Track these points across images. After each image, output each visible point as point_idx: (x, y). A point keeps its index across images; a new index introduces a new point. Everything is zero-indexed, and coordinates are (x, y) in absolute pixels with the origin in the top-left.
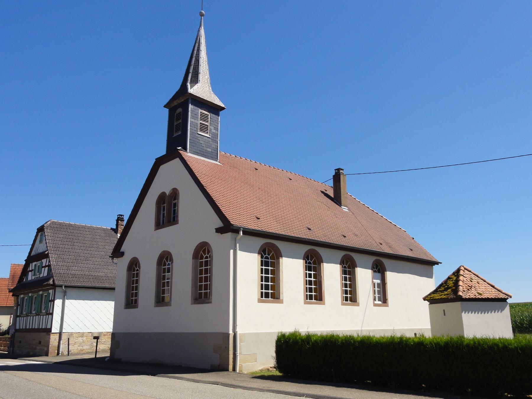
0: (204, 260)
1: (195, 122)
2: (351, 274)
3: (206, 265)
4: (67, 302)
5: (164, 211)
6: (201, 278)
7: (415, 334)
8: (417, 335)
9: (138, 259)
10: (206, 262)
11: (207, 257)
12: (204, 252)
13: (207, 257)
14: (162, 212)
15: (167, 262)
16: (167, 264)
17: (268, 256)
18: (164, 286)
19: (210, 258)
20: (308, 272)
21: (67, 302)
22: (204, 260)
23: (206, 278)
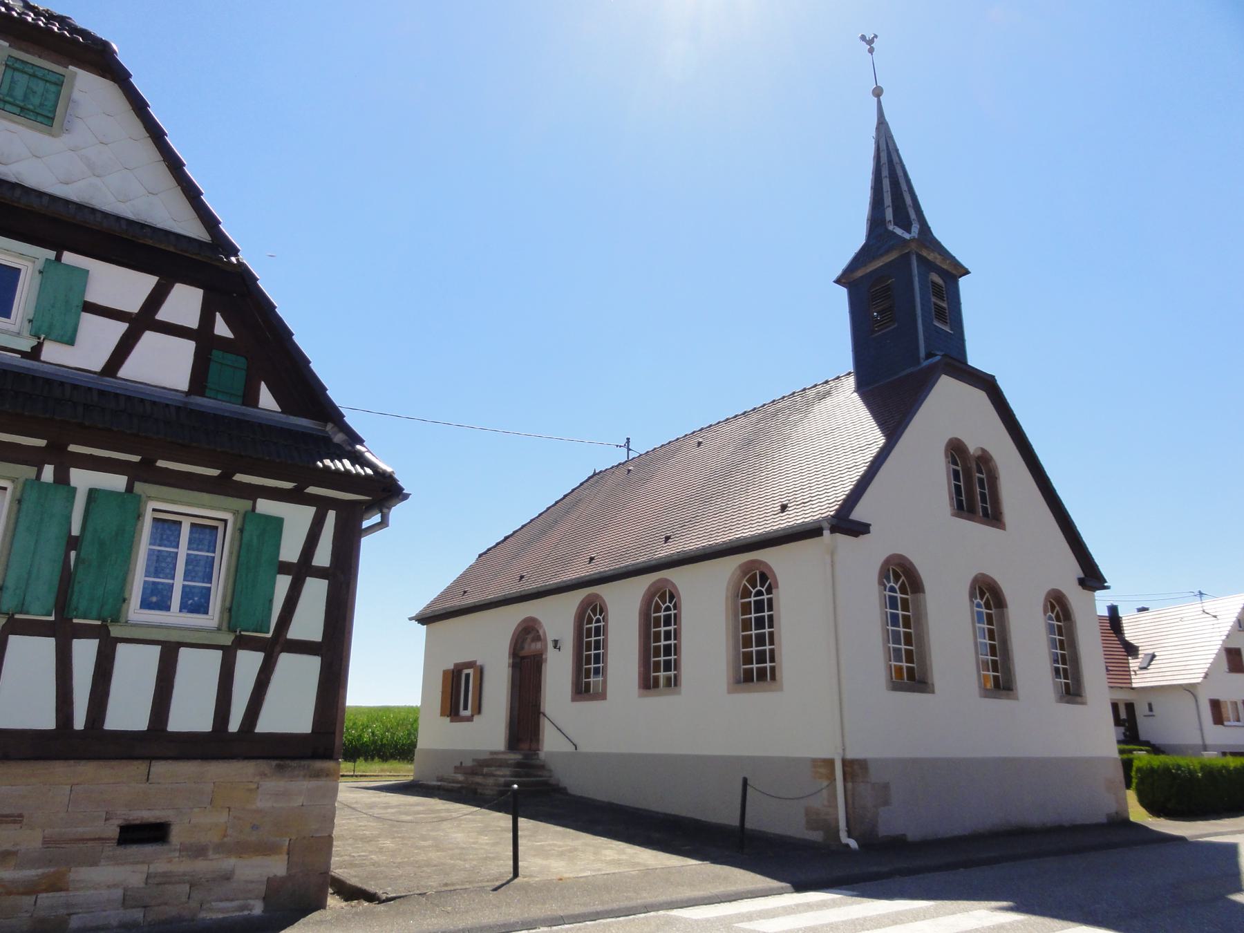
0: (753, 599)
1: (641, 455)
2: (909, 607)
3: (597, 633)
4: (735, 822)
5: (983, 495)
6: (588, 657)
7: (461, 763)
8: (463, 765)
9: (904, 556)
10: (598, 630)
11: (668, 609)
12: (662, 597)
13: (668, 609)
14: (964, 498)
15: (595, 616)
16: (595, 619)
17: (894, 585)
18: (588, 676)
19: (674, 610)
20: (672, 642)
21: (735, 822)
22: (753, 599)
23: (597, 657)
